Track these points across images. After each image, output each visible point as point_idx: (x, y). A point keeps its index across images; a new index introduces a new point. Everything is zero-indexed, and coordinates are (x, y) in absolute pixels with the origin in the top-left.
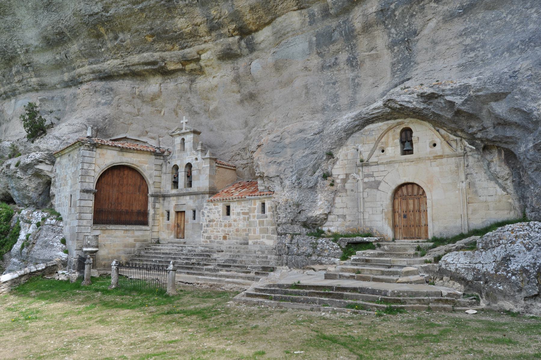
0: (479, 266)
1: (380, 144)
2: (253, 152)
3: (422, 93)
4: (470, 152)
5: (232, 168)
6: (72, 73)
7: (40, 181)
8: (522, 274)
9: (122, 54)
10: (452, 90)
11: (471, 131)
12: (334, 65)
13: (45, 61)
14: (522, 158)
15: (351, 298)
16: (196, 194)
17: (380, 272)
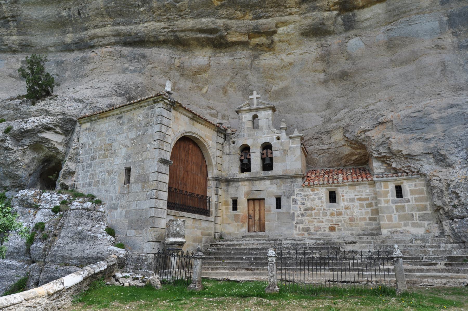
6: (82, 34)
7: (36, 156)
9: (170, 17)
13: (41, 16)
16: (282, 178)
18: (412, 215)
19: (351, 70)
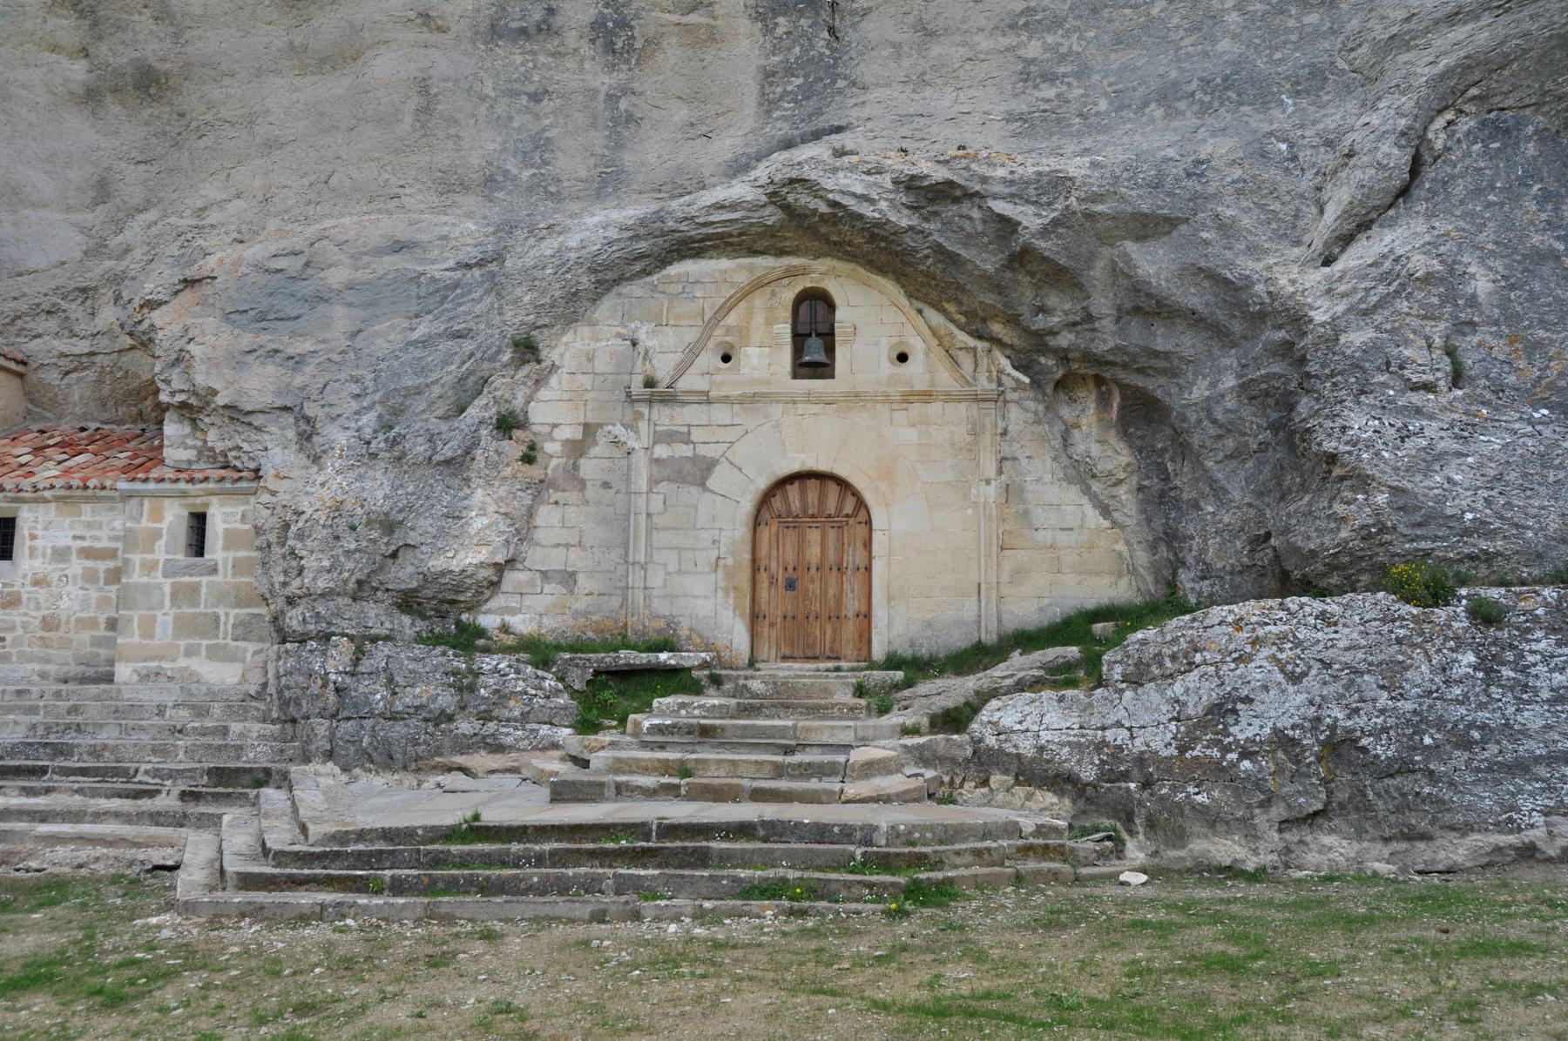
0: (1118, 736)
1: (718, 332)
2: (152, 305)
3: (913, 177)
4: (1015, 390)
5: (12, 366)
8: (1274, 752)
10: (1012, 183)
11: (1040, 322)
12: (540, 30)
14: (1193, 418)
15: (745, 861)
17: (767, 769)
18: (217, 618)
19: (168, 65)
